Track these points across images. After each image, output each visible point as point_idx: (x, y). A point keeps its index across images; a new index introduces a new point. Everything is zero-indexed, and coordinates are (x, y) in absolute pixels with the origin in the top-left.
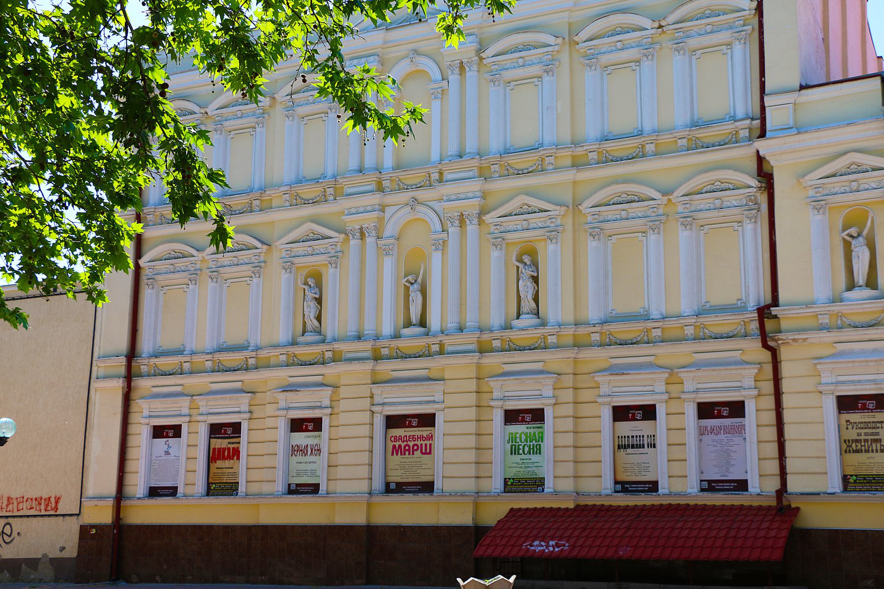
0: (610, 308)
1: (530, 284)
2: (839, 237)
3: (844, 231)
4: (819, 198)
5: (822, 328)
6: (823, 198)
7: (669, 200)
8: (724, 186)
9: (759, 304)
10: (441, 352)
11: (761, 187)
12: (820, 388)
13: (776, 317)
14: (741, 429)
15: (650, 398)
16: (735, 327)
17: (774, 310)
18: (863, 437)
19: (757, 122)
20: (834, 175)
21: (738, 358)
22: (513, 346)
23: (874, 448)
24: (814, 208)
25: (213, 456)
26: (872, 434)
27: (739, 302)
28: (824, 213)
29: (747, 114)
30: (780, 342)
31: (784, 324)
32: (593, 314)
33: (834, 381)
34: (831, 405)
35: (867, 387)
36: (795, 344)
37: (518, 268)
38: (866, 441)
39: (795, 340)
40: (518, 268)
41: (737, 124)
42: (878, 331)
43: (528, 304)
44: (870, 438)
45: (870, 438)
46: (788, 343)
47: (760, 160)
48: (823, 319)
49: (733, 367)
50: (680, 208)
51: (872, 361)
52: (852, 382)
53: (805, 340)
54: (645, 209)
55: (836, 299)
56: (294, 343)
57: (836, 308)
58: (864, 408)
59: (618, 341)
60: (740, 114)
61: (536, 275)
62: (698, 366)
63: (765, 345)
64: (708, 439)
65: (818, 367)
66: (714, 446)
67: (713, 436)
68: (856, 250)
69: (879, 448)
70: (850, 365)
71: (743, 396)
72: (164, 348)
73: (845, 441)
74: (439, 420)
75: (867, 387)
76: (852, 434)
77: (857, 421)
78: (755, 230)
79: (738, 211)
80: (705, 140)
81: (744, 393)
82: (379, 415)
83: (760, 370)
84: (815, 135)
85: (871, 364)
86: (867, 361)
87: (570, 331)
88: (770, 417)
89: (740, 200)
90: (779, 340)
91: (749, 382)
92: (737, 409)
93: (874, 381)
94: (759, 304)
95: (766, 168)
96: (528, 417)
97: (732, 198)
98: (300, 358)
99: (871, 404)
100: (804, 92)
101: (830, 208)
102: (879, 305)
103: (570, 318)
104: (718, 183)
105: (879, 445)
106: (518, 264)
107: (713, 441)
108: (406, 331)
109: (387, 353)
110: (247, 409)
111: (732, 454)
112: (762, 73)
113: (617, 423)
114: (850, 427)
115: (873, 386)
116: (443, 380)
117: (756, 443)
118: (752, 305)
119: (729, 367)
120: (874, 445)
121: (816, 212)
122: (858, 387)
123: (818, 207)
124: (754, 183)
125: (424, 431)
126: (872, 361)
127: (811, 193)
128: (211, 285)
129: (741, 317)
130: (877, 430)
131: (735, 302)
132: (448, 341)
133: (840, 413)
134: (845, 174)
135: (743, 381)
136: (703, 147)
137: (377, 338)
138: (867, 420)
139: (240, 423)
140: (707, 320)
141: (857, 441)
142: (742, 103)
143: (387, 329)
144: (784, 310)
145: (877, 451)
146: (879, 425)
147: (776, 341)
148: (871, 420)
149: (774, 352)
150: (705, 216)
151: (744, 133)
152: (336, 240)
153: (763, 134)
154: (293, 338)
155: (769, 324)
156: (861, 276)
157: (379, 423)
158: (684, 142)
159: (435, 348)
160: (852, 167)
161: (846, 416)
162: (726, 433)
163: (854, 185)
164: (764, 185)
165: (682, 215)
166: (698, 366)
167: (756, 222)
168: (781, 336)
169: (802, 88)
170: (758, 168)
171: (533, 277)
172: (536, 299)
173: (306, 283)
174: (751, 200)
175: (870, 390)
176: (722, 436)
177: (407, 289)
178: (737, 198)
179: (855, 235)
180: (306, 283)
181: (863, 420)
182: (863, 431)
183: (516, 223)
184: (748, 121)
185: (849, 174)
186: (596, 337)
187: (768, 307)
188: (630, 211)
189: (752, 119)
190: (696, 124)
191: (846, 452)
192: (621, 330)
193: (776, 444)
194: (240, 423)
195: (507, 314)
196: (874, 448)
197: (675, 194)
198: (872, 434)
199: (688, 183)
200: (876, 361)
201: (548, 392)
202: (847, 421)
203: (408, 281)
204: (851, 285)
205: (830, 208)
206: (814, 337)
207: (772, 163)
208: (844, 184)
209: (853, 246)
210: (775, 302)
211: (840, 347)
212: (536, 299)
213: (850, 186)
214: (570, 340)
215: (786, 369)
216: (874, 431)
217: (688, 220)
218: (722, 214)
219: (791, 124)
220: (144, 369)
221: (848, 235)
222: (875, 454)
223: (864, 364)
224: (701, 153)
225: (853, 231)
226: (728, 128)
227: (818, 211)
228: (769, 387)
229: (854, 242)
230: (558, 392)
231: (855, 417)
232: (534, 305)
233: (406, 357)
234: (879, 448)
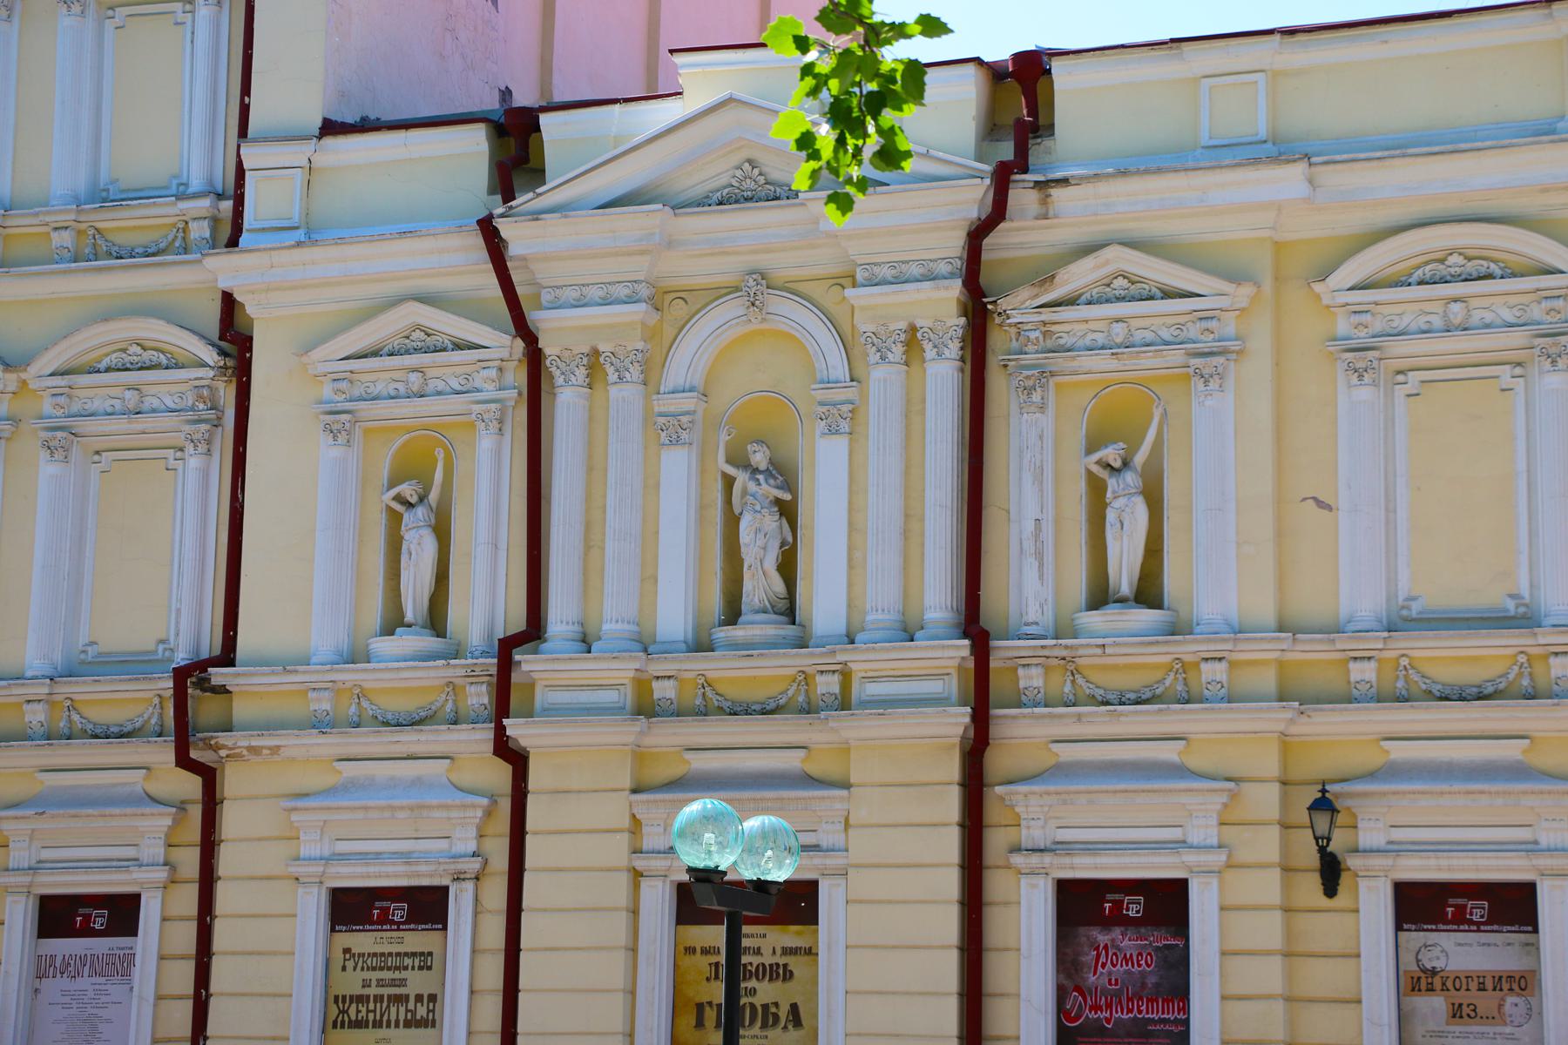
0: (83, 640)
1: (772, 522)
2: (1078, 465)
3: (1090, 451)
4: (340, 407)
5: (321, 724)
6: (348, 406)
7: (24, 382)
8: (1472, 267)
9: (197, 652)
10: (844, 703)
11: (225, 367)
12: (295, 870)
13: (223, 690)
14: (123, 967)
15: (12, 879)
16: (1159, 675)
17: (218, 675)
18: (373, 991)
19: (227, 206)
20: (375, 353)
21: (139, 789)
22: (715, 701)
23: (393, 1018)
24: (328, 429)
25: (1482, 988)
26: (393, 983)
27: (161, 647)
28: (1375, 384)
29: (211, 182)
30: (223, 753)
31: (242, 710)
32: (1361, 598)
33: (326, 853)
34: (313, 909)
35: (390, 869)
36: (254, 759)
37: (729, 482)
38: (379, 999)
39: (251, 749)
40: (729, 482)
41: (183, 205)
42: (423, 737)
43: (761, 584)
44: (386, 991)
45: (386, 991)
46: (240, 756)
47: (229, 303)
48: (319, 700)
49: (117, 811)
50: (47, 406)
51: (402, 808)
52: (363, 856)
53: (275, 750)
54: (1525, 299)
55: (356, 656)
56: (701, 645)
57: (350, 676)
58: (385, 920)
59: (1436, 689)
60: (196, 184)
61: (787, 497)
62: (41, 803)
63: (184, 761)
64: (54, 987)
65: (295, 817)
66: (66, 1006)
67: (63, 982)
68: (406, 537)
69: (402, 1018)
70: (360, 815)
71: (135, 882)
72: (102, 648)
73: (336, 998)
74: (829, 900)
75: (390, 869)
76: (351, 983)
77: (366, 950)
78: (498, 452)
79: (170, 421)
80: (120, 239)
81: (1190, 858)
82: (659, 883)
83: (177, 822)
84: (333, 251)
85: (401, 815)
86: (392, 808)
87: (1266, 649)
88: (185, 937)
89: (182, 395)
90: (224, 747)
91: (154, 849)
92: (121, 913)
93: (406, 857)
94: (197, 652)
95: (239, 321)
96: (399, 911)
97: (167, 389)
98: (721, 689)
99: (399, 911)
100: (329, 141)
101: (367, 431)
102: (432, 673)
103: (1265, 610)
104: (1120, 282)
105: (402, 1010)
106: (731, 470)
107: (64, 993)
108: (383, 645)
109: (671, 694)
110: (472, 846)
111: (101, 1027)
112: (246, 89)
113: (681, 928)
114: (350, 964)
115: (402, 869)
116: (846, 785)
117: (151, 999)
118: (181, 655)
119: (108, 811)
120: (393, 1010)
121: (1354, 379)
122: (372, 869)
123: (1552, 350)
124: (210, 356)
125: (416, 940)
126: (402, 808)
127: (327, 391)
128: (48, 469)
129: (798, 662)
130: (404, 974)
131: (152, 647)
132: (860, 661)
133: (333, 930)
134: (1099, 302)
135: (133, 848)
136: (109, 255)
137: (645, 644)
138: (386, 949)
139: (136, 898)
140: (80, 689)
141: (360, 999)
142: (198, 157)
143: (673, 619)
144: (244, 675)
145: (397, 1025)
146: (408, 961)
147: (216, 748)
148: (395, 949)
149: (209, 777)
150: (107, 429)
151: (199, 231)
152: (1223, 302)
153: (233, 242)
154: (697, 627)
155: (204, 708)
156: (761, 584)
157: (658, 901)
158: (65, 239)
159: (828, 685)
160: (1452, 260)
161: (347, 939)
162: (95, 973)
163: (1119, 332)
164: (230, 363)
165: (328, 407)
166: (41, 803)
167: (209, 452)
168: (224, 738)
169: (330, 128)
170: (222, 321)
171: (778, 502)
172: (788, 567)
173: (746, 465)
174: (200, 397)
175: (396, 876)
176: (85, 983)
177: (395, 520)
178: (1513, 300)
179: (1117, 464)
180: (746, 465)
181: (378, 949)
182: (374, 976)
183: (1428, 307)
184: (206, 203)
185: (408, 352)
186: (36, 716)
187: (201, 666)
188: (431, 373)
189: (220, 196)
190: (103, 197)
191: (335, 1026)
192: (1448, 658)
193: (189, 1004)
194: (136, 898)
195: (698, 614)
196: (393, 1018)
197: (33, 369)
198: (393, 983)
199: (64, 344)
200: (411, 809)
201: (1203, 830)
202: (347, 951)
203: (399, 499)
204: (393, 623)
205: (367, 431)
206: (293, 743)
207: (250, 310)
208: (396, 375)
209: (1109, 495)
210: (227, 657)
211: (350, 770)
212: (788, 567)
213: (1445, 314)
214: (1267, 681)
215: (231, 821)
216: (397, 975)
217: (62, 437)
218: (139, 427)
219: (296, 219)
220: (1031, 679)
221: (1097, 463)
222: (392, 1032)
223: (387, 814)
224: (100, 270)
225: (1111, 454)
226: (166, 213)
227: (335, 438)
228: (190, 860)
229: (1112, 483)
230: (1231, 833)
231: (364, 941)
232: (779, 586)
233: (738, 710)
234: (402, 1018)
